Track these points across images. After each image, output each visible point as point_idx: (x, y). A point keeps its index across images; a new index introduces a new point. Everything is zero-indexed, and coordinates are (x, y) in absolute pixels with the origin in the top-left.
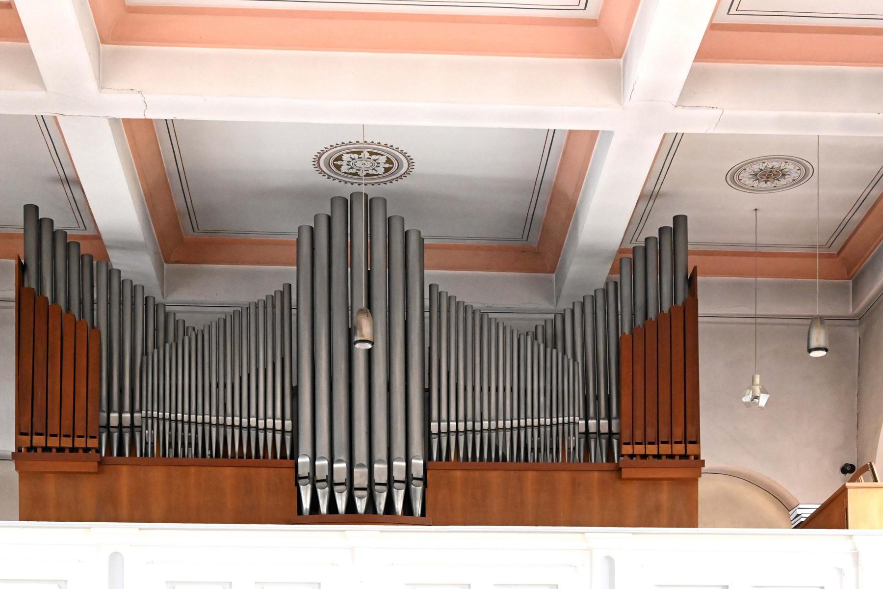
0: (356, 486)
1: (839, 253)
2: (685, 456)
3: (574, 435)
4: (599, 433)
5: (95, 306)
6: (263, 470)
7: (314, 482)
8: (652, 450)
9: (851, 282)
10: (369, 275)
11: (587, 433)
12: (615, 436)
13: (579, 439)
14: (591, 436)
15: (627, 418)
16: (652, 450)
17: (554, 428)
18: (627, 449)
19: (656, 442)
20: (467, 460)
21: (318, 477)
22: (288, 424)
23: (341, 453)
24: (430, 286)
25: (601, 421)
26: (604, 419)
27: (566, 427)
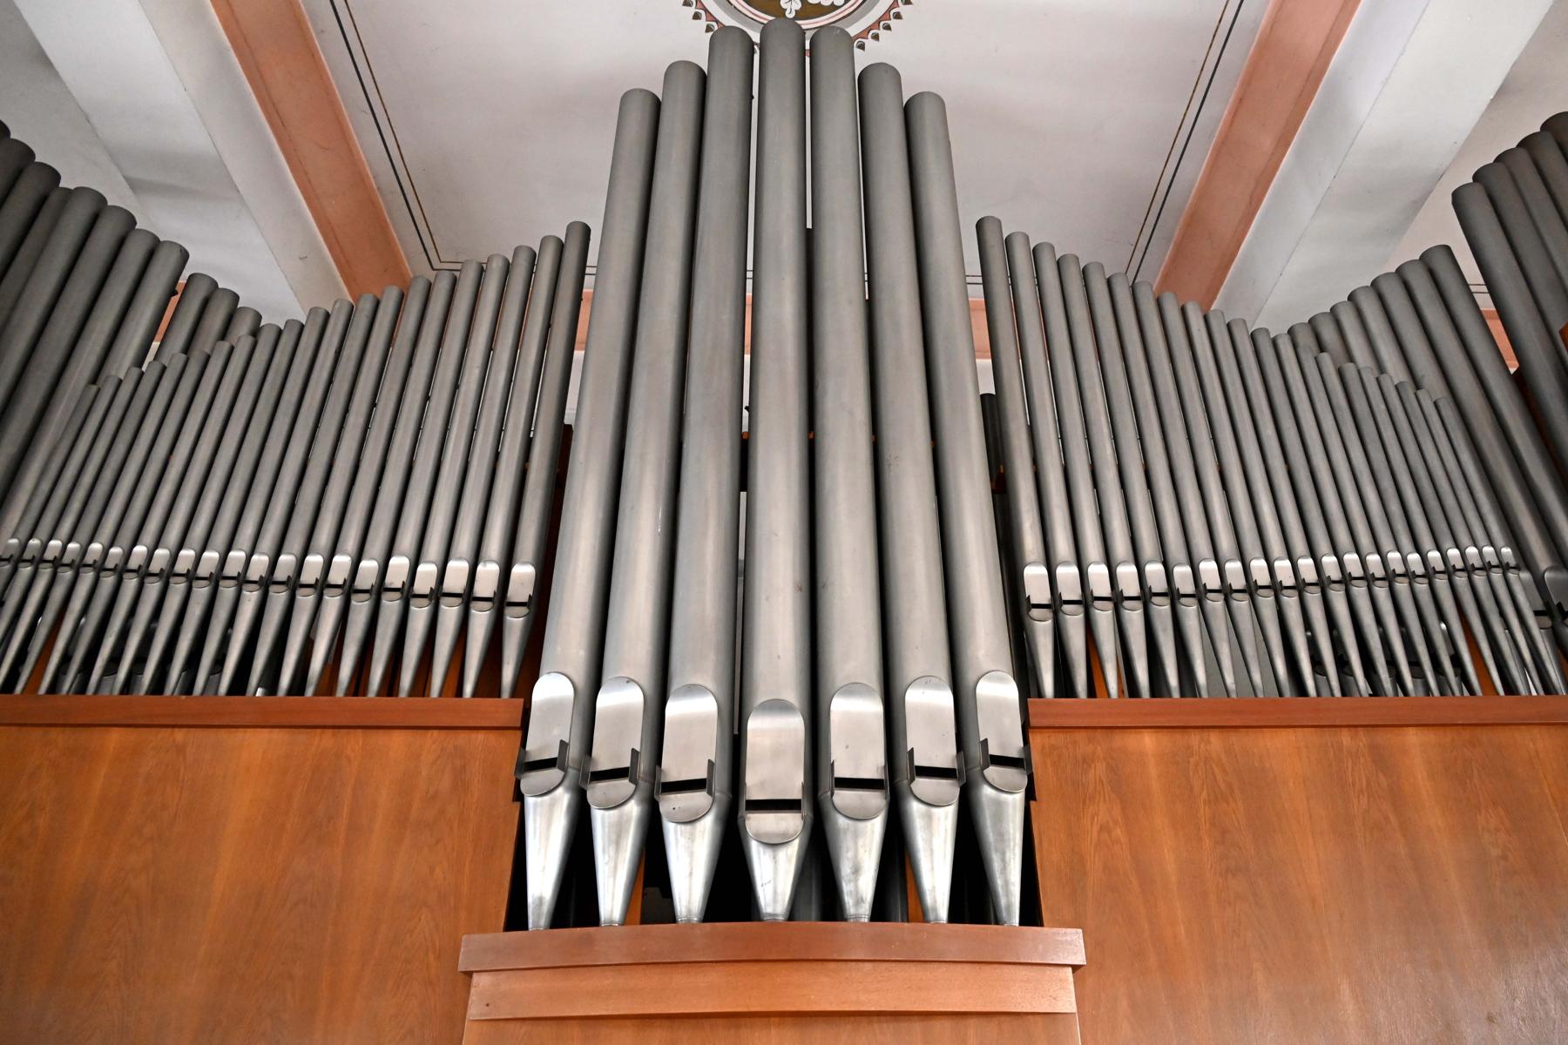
0: (754, 792)
6: (398, 738)
7: (586, 778)
10: (810, 242)
21: (674, 769)
22: (524, 572)
23: (700, 660)
24: (980, 226)
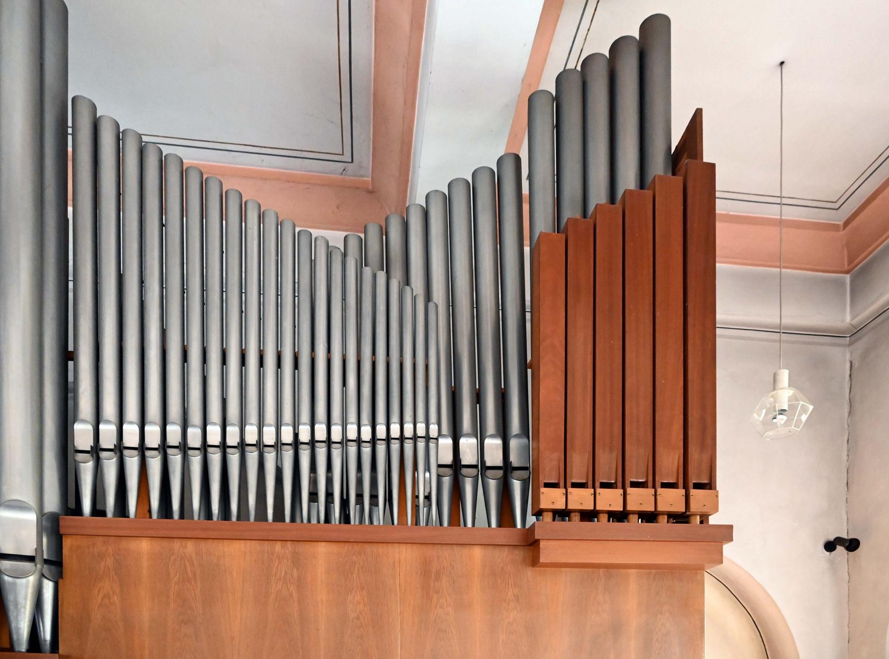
1: (847, 223)
2: (681, 518)
3: (428, 468)
4: (482, 468)
5: (70, 395)
8: (610, 500)
9: (848, 277)
11: (456, 465)
12: (517, 473)
13: (439, 477)
14: (464, 471)
15: (550, 428)
16: (610, 500)
17: (381, 448)
18: (552, 498)
19: (622, 483)
20: (283, 520)
25: (488, 441)
26: (492, 436)
27: (408, 446)
